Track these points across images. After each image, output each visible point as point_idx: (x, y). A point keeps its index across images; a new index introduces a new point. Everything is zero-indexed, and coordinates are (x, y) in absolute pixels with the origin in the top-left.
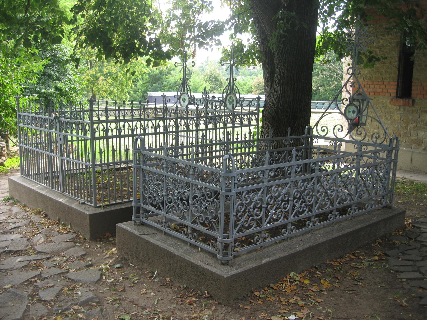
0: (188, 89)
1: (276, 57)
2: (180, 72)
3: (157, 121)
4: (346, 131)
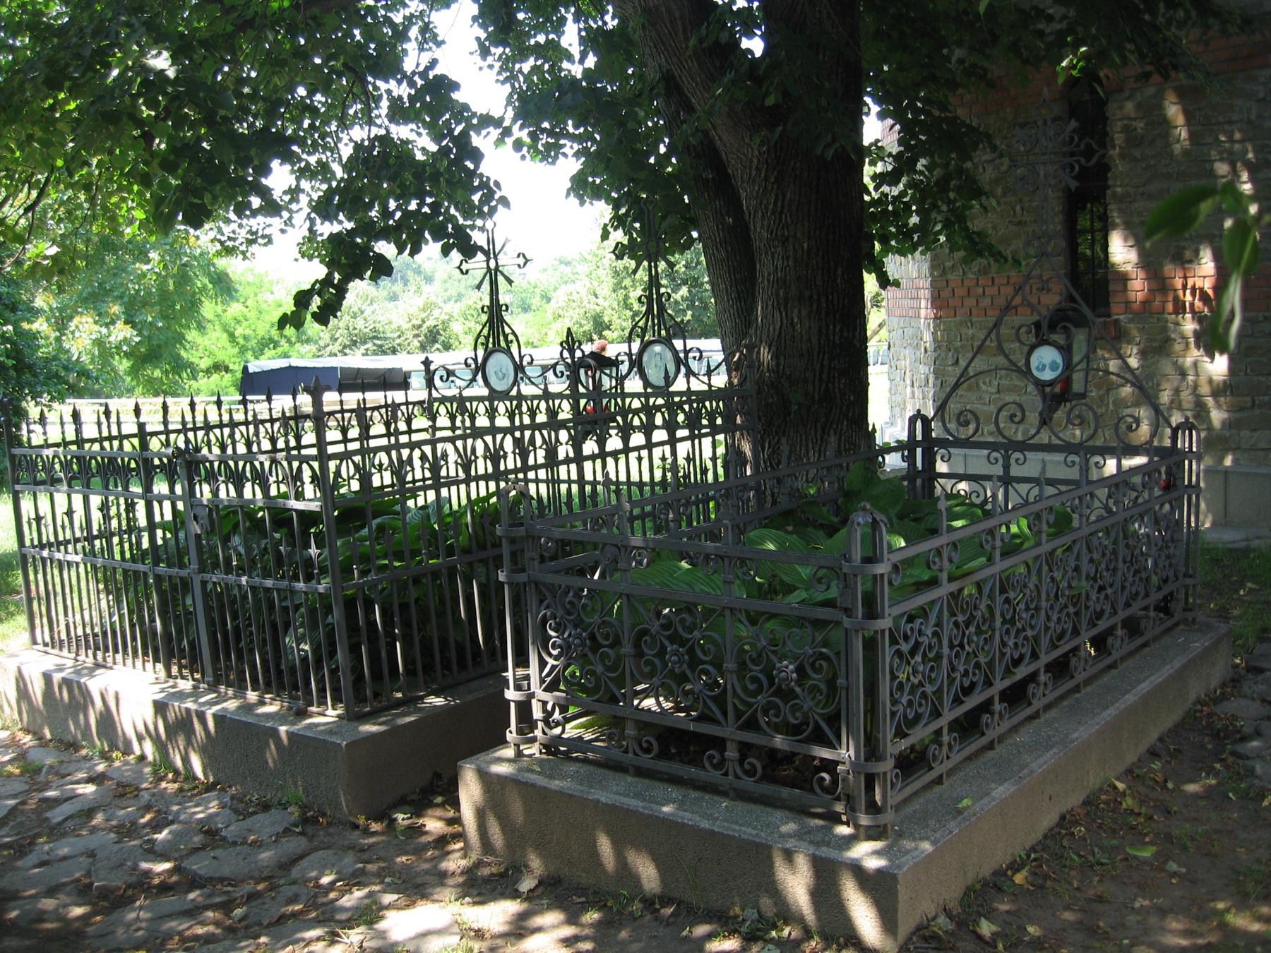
0: (511, 337)
1: (759, 225)
2: (479, 287)
3: (470, 441)
4: (1033, 418)
